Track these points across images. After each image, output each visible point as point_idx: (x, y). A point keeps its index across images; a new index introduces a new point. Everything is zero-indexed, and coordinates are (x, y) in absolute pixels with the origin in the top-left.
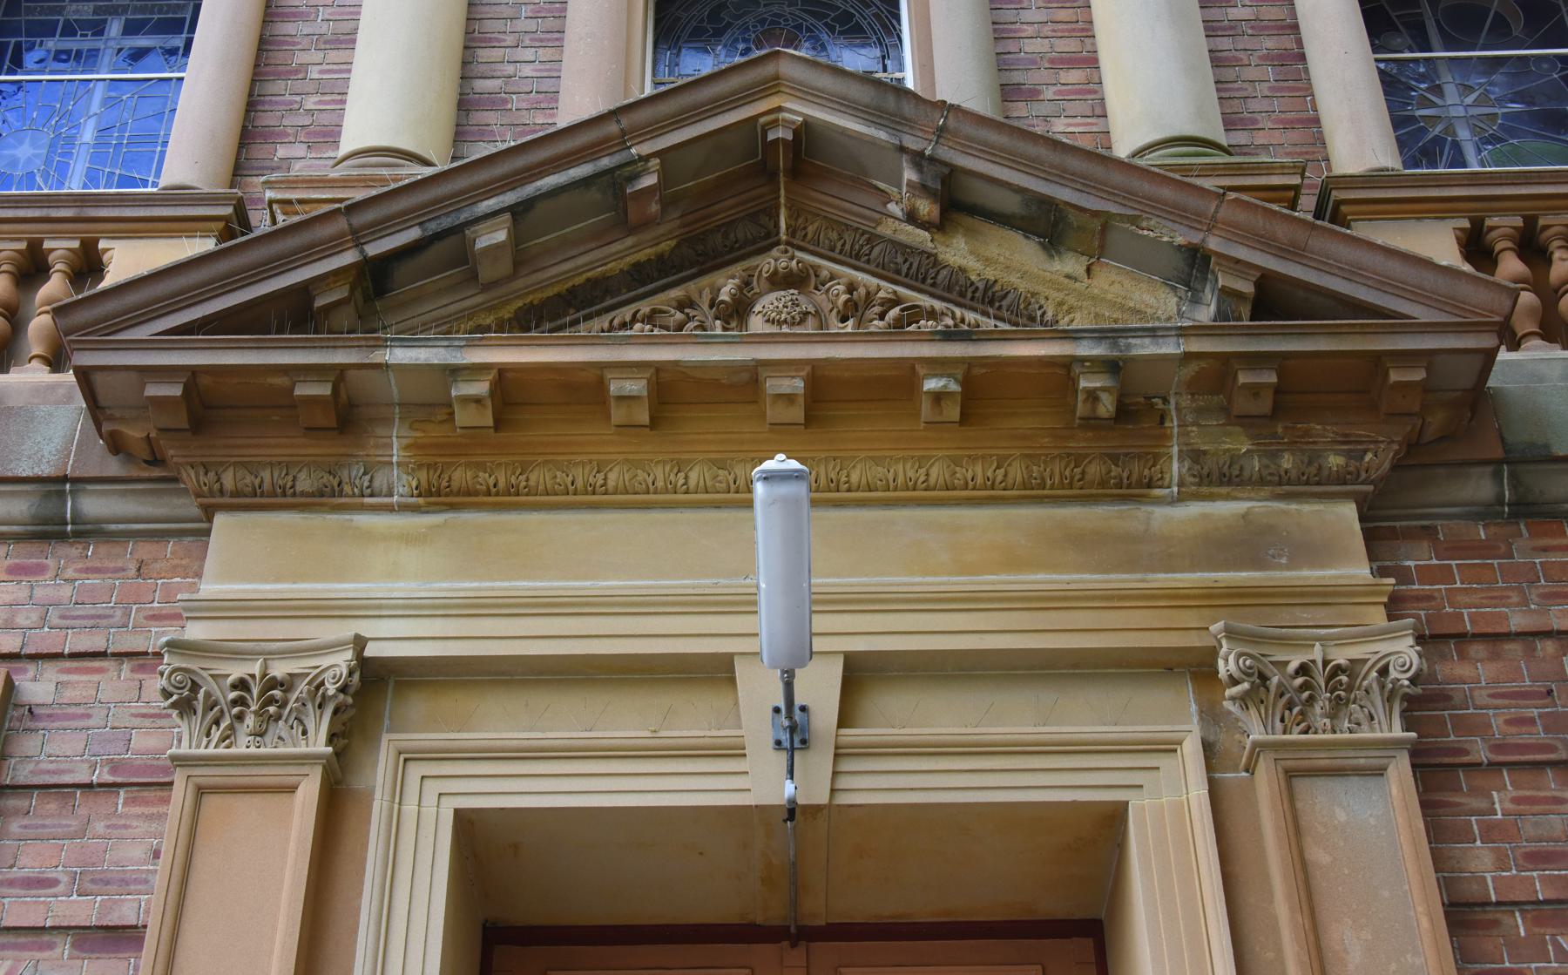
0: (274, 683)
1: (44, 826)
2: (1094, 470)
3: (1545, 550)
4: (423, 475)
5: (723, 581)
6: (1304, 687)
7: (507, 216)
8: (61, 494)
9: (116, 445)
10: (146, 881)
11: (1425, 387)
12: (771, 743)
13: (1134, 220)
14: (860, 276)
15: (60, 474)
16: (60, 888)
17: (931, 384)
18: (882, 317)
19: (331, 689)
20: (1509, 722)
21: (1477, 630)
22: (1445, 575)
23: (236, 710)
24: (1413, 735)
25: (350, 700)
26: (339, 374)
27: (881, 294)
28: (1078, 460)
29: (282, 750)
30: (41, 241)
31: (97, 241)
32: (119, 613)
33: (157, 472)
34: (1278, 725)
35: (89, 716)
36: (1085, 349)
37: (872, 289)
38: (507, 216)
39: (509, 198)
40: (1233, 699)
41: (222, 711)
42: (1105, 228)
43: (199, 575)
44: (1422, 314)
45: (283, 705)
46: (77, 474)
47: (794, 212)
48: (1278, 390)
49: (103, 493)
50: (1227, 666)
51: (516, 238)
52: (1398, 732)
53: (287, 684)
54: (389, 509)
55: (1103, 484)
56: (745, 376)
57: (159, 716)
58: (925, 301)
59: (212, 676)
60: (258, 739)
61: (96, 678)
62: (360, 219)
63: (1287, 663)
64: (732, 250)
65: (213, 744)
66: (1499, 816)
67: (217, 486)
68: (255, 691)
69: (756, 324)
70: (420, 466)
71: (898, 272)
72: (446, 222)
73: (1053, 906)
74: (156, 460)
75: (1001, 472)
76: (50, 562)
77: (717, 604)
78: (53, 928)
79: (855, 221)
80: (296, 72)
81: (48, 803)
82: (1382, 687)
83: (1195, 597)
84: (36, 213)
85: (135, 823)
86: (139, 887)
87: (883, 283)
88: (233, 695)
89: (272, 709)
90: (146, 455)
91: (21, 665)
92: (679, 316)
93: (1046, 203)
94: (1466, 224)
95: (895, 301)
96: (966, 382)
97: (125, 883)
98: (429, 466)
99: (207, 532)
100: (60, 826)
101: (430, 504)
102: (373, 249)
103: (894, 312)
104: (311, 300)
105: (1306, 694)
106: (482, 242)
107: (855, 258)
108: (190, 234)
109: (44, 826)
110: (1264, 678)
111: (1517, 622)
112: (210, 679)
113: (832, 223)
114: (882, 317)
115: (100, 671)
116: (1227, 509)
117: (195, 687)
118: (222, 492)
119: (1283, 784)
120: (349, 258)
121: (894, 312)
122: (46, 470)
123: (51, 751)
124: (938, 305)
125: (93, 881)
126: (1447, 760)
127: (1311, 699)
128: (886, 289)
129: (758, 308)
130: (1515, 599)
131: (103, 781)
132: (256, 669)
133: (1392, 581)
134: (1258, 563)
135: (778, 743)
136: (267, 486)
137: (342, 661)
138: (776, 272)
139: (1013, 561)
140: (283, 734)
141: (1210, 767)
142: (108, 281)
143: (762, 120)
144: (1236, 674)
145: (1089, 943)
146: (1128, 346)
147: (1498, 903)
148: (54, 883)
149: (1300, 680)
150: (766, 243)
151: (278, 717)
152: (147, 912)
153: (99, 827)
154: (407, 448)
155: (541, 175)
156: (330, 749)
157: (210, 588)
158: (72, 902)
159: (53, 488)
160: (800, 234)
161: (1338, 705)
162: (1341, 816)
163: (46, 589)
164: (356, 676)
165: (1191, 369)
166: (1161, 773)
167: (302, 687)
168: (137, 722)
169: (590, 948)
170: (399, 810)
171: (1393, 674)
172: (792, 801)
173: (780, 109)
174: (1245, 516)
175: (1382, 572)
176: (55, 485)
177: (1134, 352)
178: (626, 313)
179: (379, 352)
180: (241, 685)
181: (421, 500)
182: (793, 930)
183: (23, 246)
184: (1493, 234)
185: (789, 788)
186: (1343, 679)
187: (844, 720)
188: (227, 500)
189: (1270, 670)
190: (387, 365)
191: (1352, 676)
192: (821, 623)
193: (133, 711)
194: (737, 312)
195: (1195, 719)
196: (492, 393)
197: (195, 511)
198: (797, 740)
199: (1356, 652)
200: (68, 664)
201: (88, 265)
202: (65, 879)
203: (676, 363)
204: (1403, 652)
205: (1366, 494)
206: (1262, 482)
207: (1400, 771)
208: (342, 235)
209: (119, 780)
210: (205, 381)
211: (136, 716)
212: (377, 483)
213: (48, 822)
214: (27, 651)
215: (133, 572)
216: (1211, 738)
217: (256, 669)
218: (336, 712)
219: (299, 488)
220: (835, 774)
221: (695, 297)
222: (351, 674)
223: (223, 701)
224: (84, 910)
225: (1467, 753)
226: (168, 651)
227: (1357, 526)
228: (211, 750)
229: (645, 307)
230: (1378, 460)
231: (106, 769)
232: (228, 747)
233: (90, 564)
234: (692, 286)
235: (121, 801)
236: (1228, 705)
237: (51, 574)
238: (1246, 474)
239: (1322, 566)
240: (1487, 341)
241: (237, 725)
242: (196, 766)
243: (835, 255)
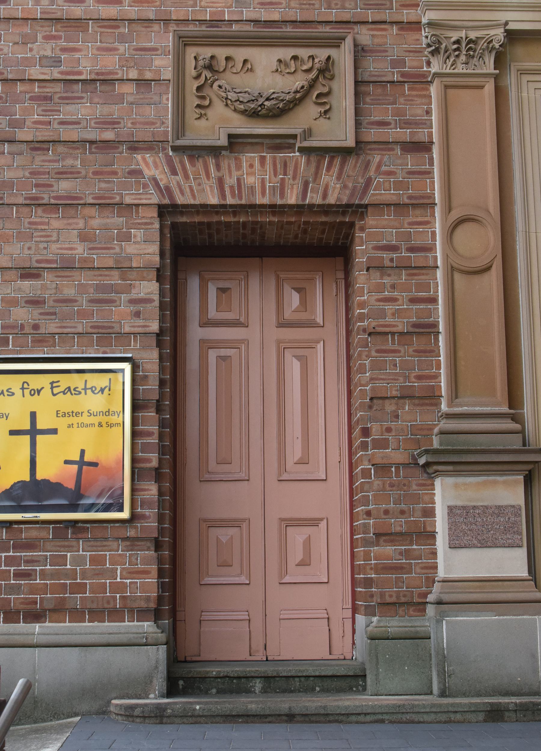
0: (470, 41)
1: (379, 100)
16: (392, 126)
35: (387, 51)
41: (450, 53)
45: (475, 51)
53: (474, 42)
59: (444, 37)
60: (466, 65)
61: (384, 33)
65: (448, 68)
68: (464, 45)
81: (377, 89)
85: (416, 99)
86: (424, 126)
91: (351, 26)
100: (386, 100)
109: (379, 100)
112: (444, 39)
119: (443, 90)
123: (375, 67)
125: (405, 123)
131: (91, 79)
140: (476, 64)
149: (455, 46)
151: (473, 57)
158: (398, 131)
167: (482, 44)
168: (407, 54)
170: (521, 95)
180: (458, 42)
193: (405, 49)
200: (371, 26)
209: (405, 80)
213: (381, 98)
217: (463, 34)
223: (450, 49)
224: (405, 134)
226: (428, 27)
228: (448, 71)
231: (399, 75)
232: (453, 69)
241: (457, 60)
242: (443, 77)
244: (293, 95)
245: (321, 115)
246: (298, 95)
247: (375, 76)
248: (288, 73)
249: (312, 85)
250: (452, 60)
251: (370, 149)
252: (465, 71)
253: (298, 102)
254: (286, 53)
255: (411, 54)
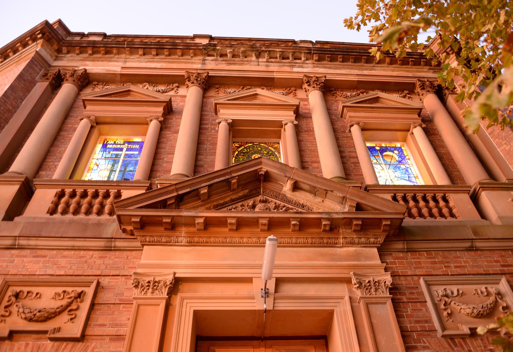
0: (156, 282)
2: (325, 241)
3: (414, 258)
4: (188, 239)
5: (250, 262)
6: (370, 285)
7: (207, 187)
8: (16, 240)
9: (124, 231)
10: (126, 325)
11: (390, 225)
12: (261, 296)
13: (332, 191)
14: (277, 201)
15: (112, 237)
16: (107, 326)
17: (293, 222)
18: (282, 209)
19: (168, 283)
20: (409, 293)
21: (402, 274)
22: (395, 263)
23: (147, 288)
24: (392, 296)
25: (172, 286)
26: (173, 217)
27: (281, 205)
28: (322, 238)
29: (157, 297)
30: (109, 190)
31: (120, 190)
32: (122, 267)
33: (132, 237)
34: (365, 293)
35: (115, 289)
36: (324, 216)
37: (280, 204)
38: (207, 187)
39: (208, 183)
40: (355, 288)
42: (326, 193)
43: (140, 259)
44: (389, 211)
45: (158, 286)
46: (115, 237)
47: (264, 189)
48: (362, 225)
49: (119, 241)
50: (354, 281)
51: (208, 191)
52: (388, 295)
53: (159, 282)
54: (181, 246)
55: (327, 243)
56: (256, 220)
57: (130, 289)
58: (290, 206)
61: (117, 280)
62: (178, 186)
63: (365, 281)
64: (251, 195)
66: (409, 313)
67: (145, 240)
68: (152, 284)
69: (257, 210)
70: (188, 237)
71: (285, 200)
72: (195, 188)
73: (317, 333)
74: (132, 234)
75: (306, 241)
76: (108, 256)
77: (245, 267)
78: (105, 335)
79: (276, 190)
80: (162, 159)
82: (385, 286)
83: (347, 267)
84: (109, 184)
87: (282, 203)
88: (147, 284)
89: (155, 288)
90: (130, 233)
92: (241, 208)
93: (315, 187)
94: (393, 195)
95: (284, 206)
96: (300, 222)
97: (121, 325)
98: (190, 237)
99: (142, 250)
101: (189, 245)
102: (180, 192)
103: (284, 209)
104: (167, 202)
105: (370, 287)
106: (202, 192)
107: (276, 197)
108: (140, 189)
110: (361, 284)
111: (409, 273)
113: (271, 191)
114: (282, 209)
115: (117, 279)
116: (351, 249)
117: (139, 283)
118: (146, 241)
120: (175, 194)
121: (284, 209)
122: (109, 236)
124: (293, 207)
125: (114, 325)
126: (398, 301)
127: (371, 288)
128: (282, 204)
129: (257, 207)
130: (409, 268)
132: (152, 279)
133: (385, 264)
134: (358, 260)
135: (262, 296)
136: (156, 240)
137: (170, 278)
138: (260, 200)
139: (310, 259)
141: (351, 302)
142: (123, 198)
143: (258, 170)
144: (356, 283)
145: (324, 340)
146: (332, 216)
147: (411, 331)
148: (105, 325)
150: (258, 194)
151: (157, 289)
152: (126, 332)
153: (116, 313)
154: (185, 233)
155: (214, 179)
156: (167, 297)
157: (143, 261)
159: (15, 238)
160: (265, 193)
161: (376, 290)
162: (378, 313)
163: (107, 261)
164: (174, 281)
165: (344, 221)
166: (341, 303)
168: (125, 290)
169: (219, 341)
171: (387, 283)
172: (266, 309)
173: (262, 168)
174: (355, 251)
175: (382, 262)
176: (111, 239)
177: (333, 217)
178: (230, 207)
179: (181, 213)
180: (149, 282)
181: (188, 244)
182: (262, 338)
183: (105, 191)
184: (398, 197)
185: (265, 306)
186: (377, 284)
187: (276, 291)
188: (147, 243)
189: (362, 282)
190: (183, 216)
191: (379, 283)
192: (275, 271)
194: (254, 207)
195: (347, 292)
196: (204, 222)
197: (141, 246)
198: (266, 295)
199: (379, 278)
201: (118, 195)
202: (108, 324)
203: (242, 217)
204: (388, 278)
205: (379, 246)
206: (358, 244)
207: (389, 303)
208: (173, 190)
209: (121, 303)
210: (144, 218)
211: (125, 289)
212: (179, 240)
214: (102, 274)
215: (126, 258)
216: (351, 296)
217: (152, 279)
218: (169, 288)
219: (162, 241)
220: (274, 303)
221: (244, 204)
222: (172, 280)
224: (112, 331)
225: (402, 299)
227: (377, 253)
228: (142, 296)
229: (234, 206)
230: (381, 240)
233: (117, 256)
234: (243, 203)
235: (121, 307)
236: (354, 289)
237: (108, 258)
238: (355, 242)
239: (371, 261)
240: (401, 216)
241: (147, 291)
243: (272, 197)
244: (55, 310)
245: (68, 321)
246: (58, 310)
247: (106, 301)
248: (59, 299)
249: (70, 304)
250: (145, 291)
251: (92, 339)
252: (151, 297)
253: (57, 314)
254: (60, 290)
255: (128, 290)
